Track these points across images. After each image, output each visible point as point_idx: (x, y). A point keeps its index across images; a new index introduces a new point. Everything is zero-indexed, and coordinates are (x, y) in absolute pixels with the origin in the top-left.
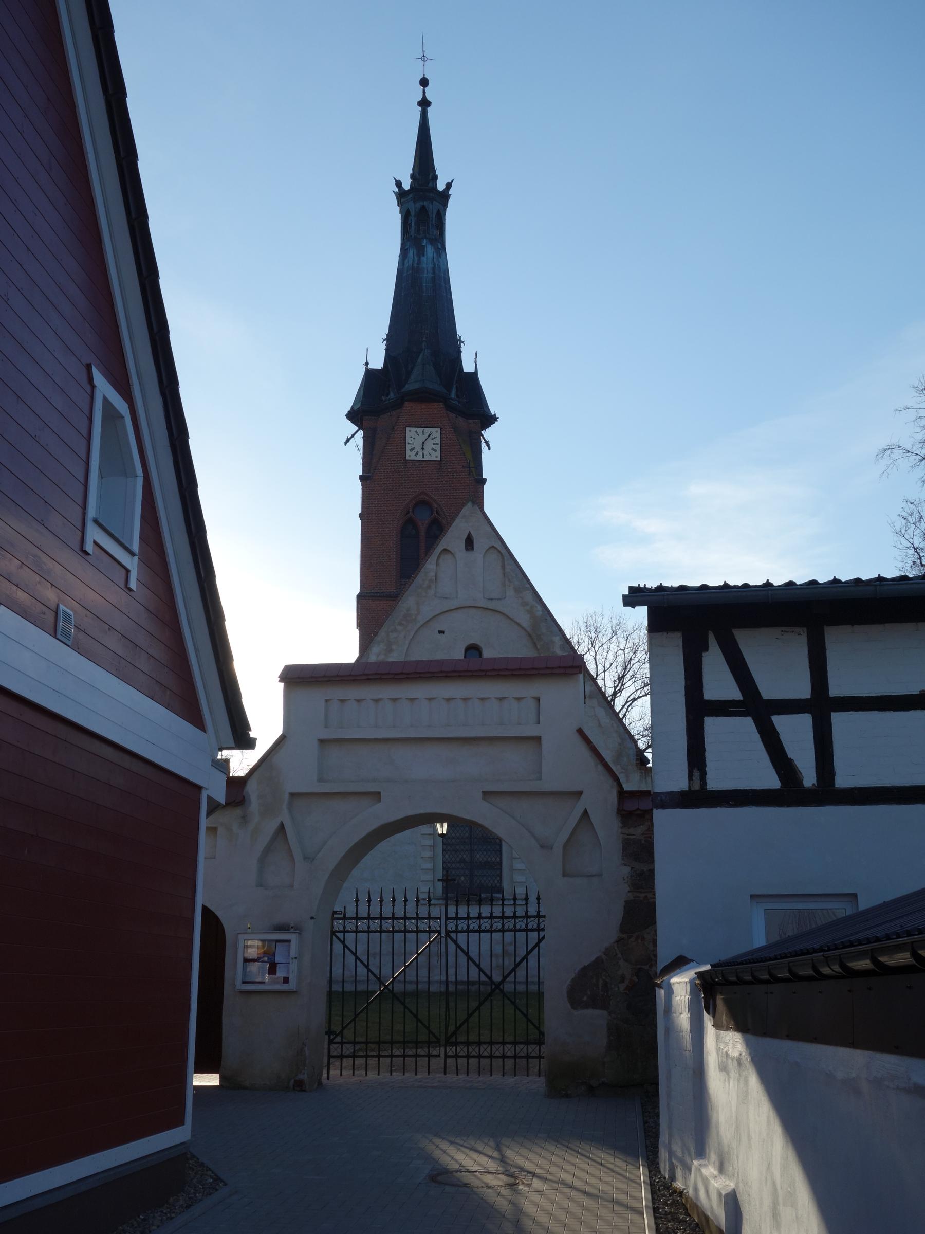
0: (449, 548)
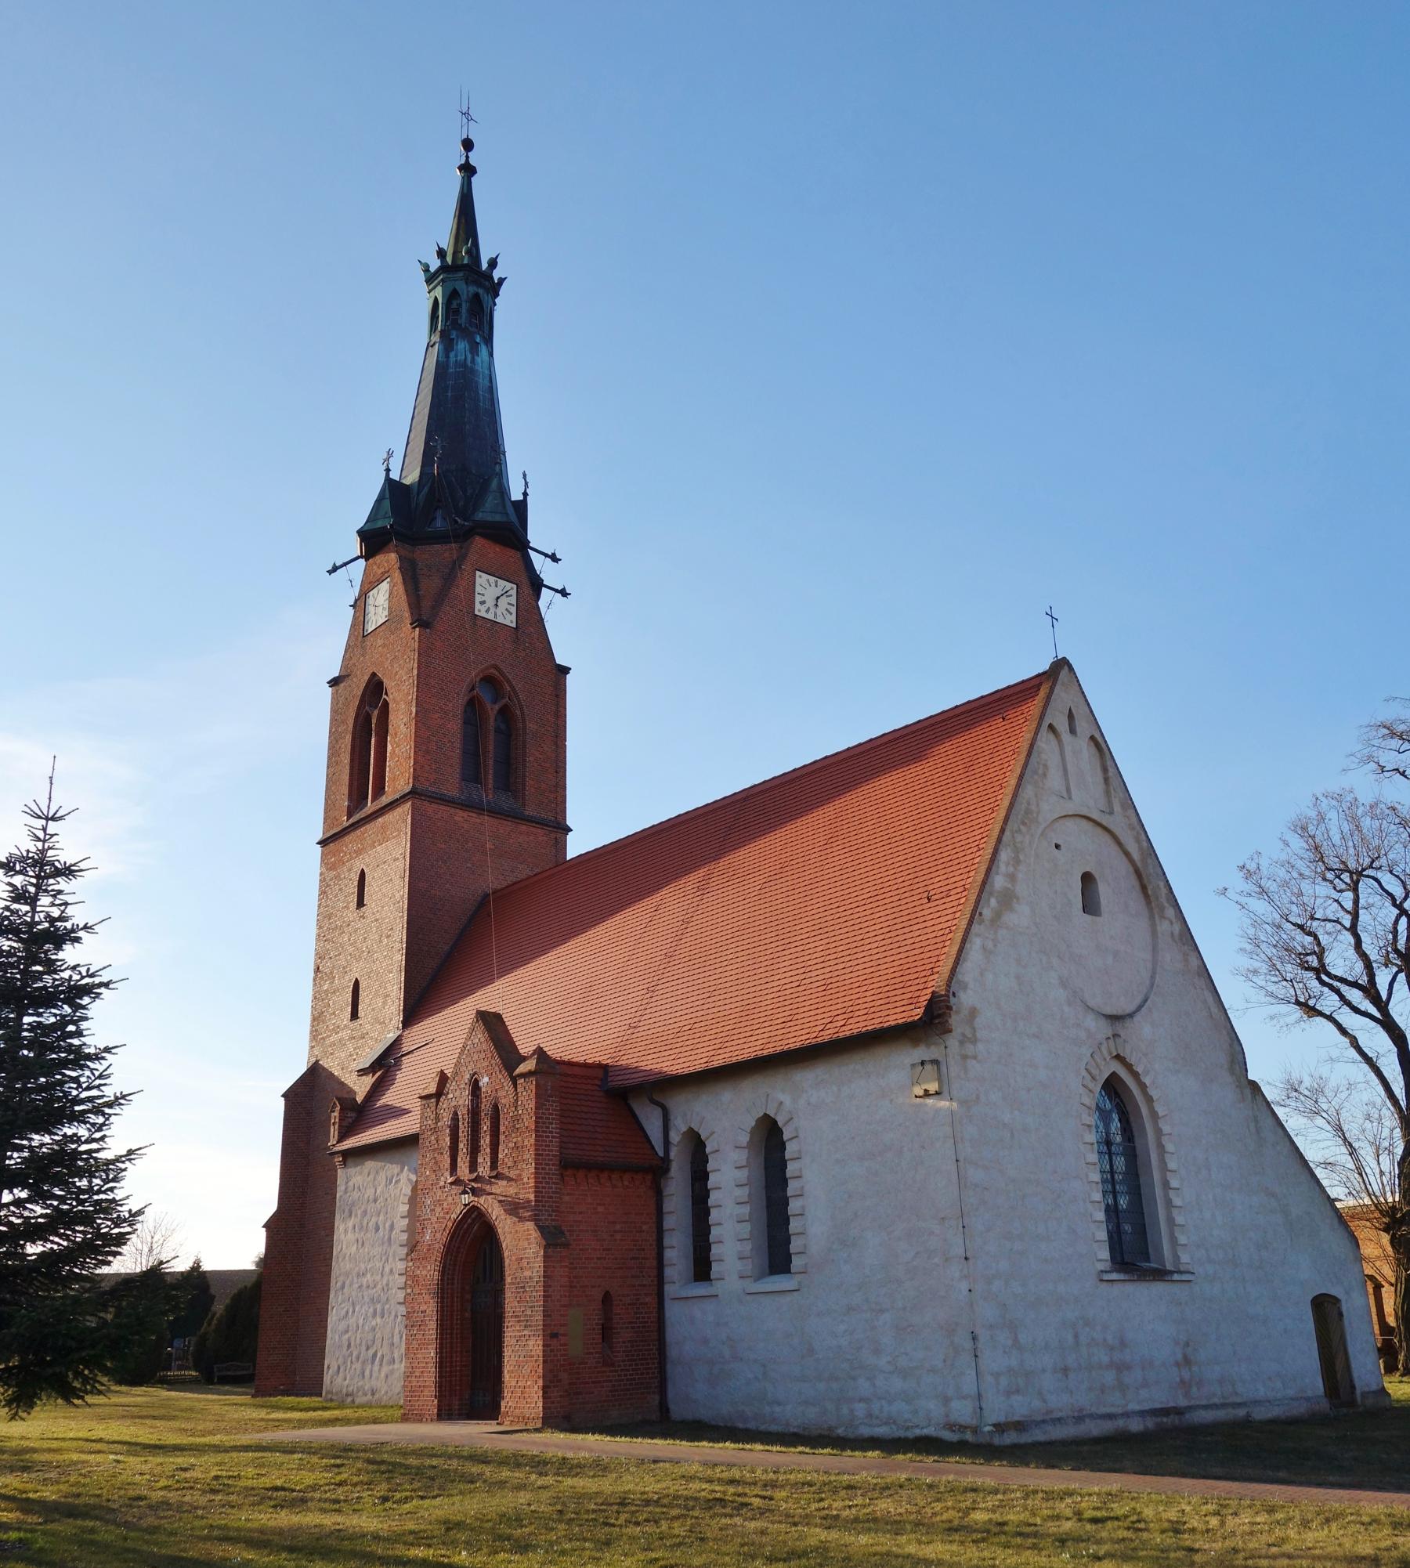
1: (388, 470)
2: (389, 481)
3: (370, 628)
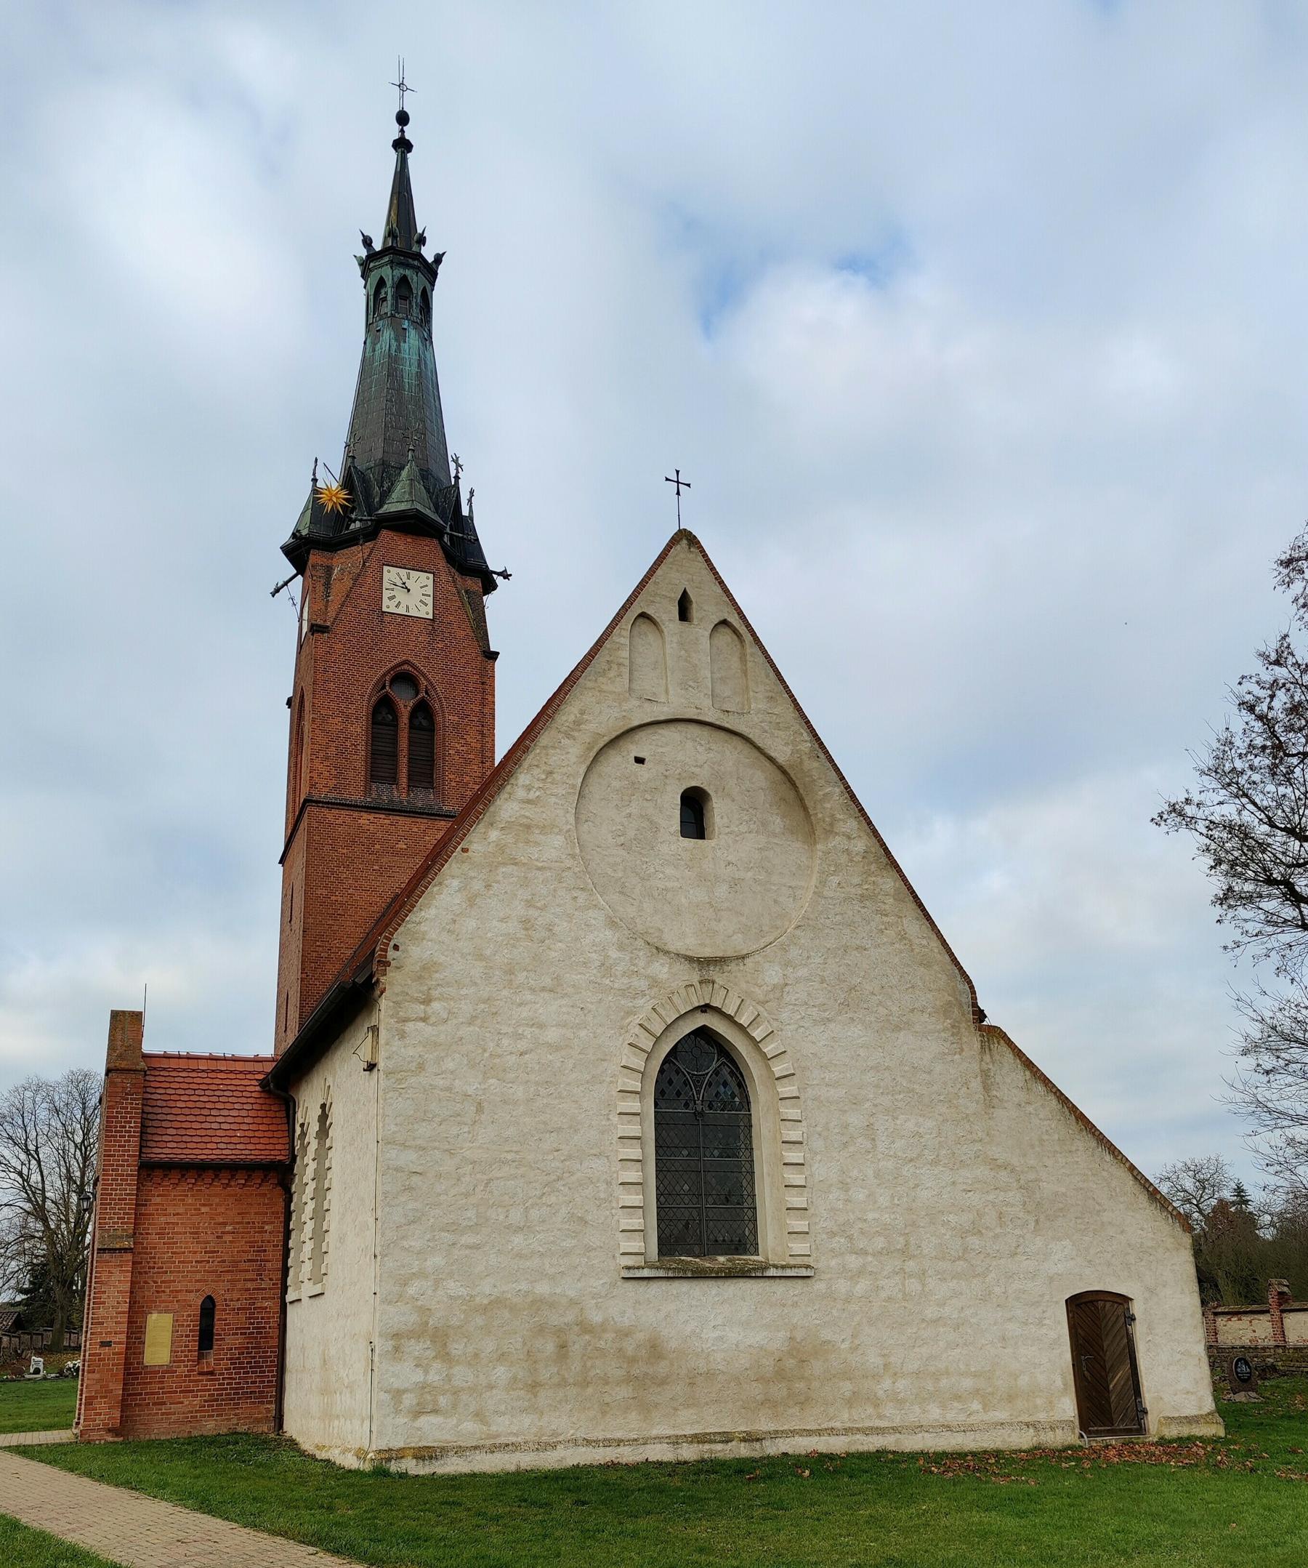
0: (650, 612)
1: (315, 480)
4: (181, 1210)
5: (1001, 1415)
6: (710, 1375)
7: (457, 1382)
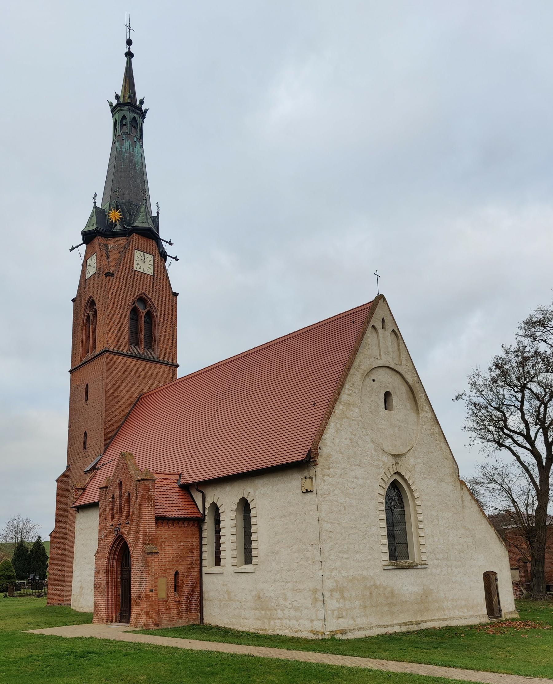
1: (95, 203)
2: (95, 207)
3: (88, 276)
4: (166, 537)
5: (471, 613)
6: (406, 602)
7: (347, 607)
